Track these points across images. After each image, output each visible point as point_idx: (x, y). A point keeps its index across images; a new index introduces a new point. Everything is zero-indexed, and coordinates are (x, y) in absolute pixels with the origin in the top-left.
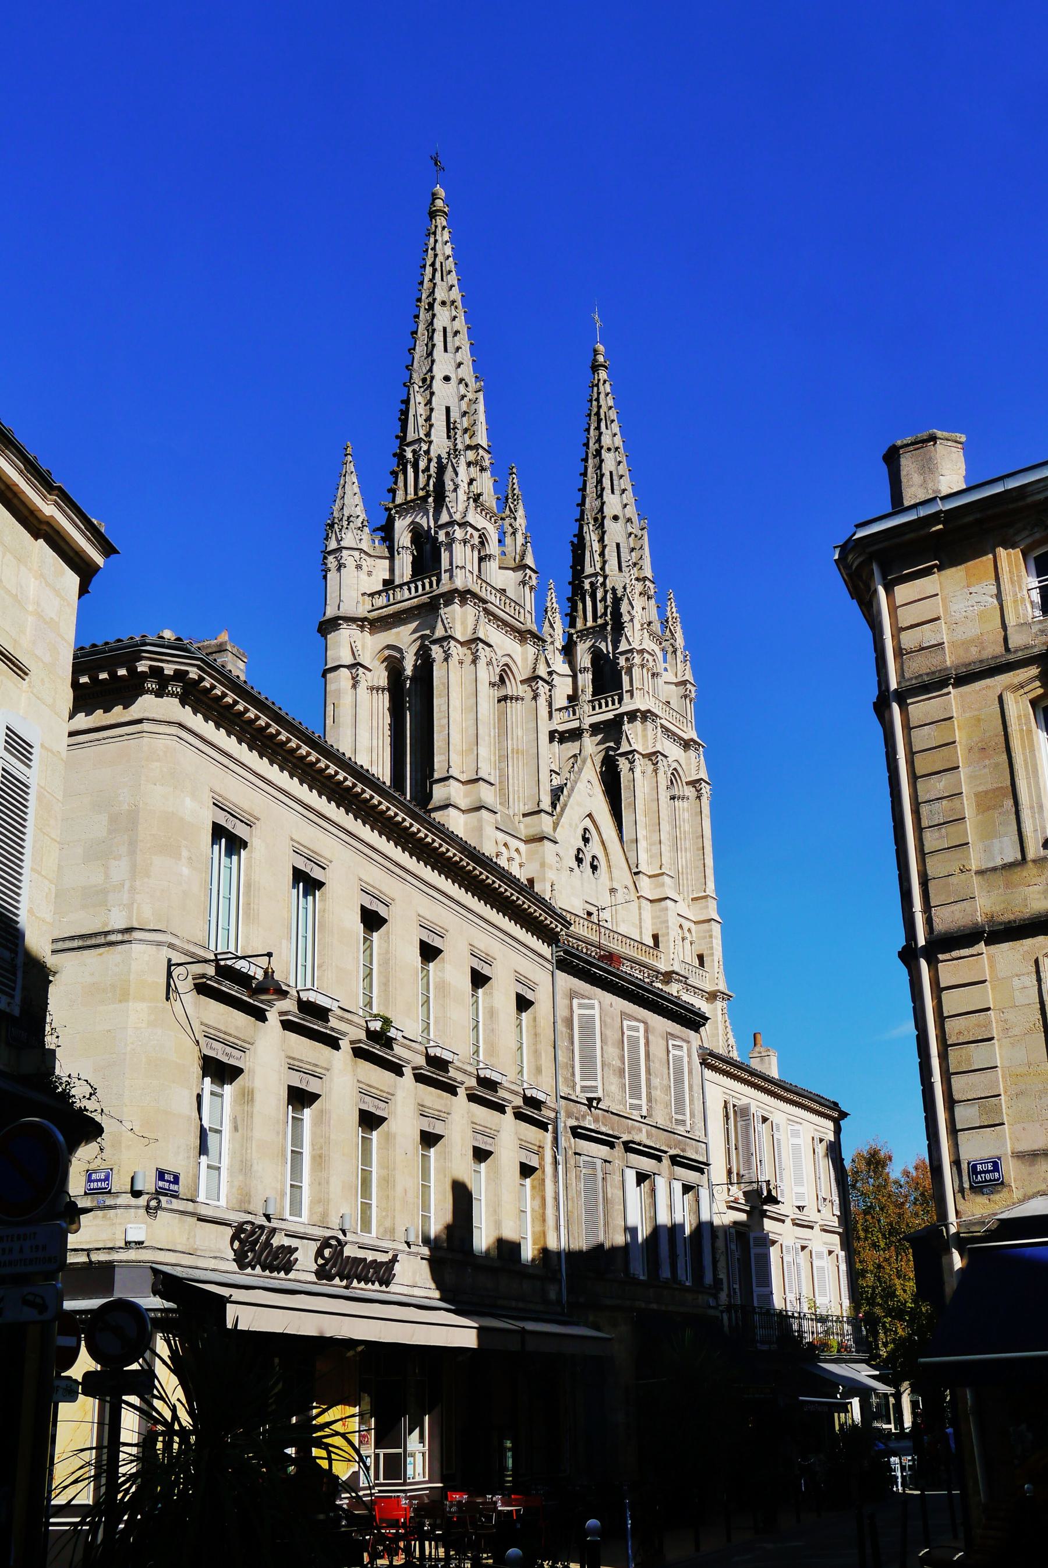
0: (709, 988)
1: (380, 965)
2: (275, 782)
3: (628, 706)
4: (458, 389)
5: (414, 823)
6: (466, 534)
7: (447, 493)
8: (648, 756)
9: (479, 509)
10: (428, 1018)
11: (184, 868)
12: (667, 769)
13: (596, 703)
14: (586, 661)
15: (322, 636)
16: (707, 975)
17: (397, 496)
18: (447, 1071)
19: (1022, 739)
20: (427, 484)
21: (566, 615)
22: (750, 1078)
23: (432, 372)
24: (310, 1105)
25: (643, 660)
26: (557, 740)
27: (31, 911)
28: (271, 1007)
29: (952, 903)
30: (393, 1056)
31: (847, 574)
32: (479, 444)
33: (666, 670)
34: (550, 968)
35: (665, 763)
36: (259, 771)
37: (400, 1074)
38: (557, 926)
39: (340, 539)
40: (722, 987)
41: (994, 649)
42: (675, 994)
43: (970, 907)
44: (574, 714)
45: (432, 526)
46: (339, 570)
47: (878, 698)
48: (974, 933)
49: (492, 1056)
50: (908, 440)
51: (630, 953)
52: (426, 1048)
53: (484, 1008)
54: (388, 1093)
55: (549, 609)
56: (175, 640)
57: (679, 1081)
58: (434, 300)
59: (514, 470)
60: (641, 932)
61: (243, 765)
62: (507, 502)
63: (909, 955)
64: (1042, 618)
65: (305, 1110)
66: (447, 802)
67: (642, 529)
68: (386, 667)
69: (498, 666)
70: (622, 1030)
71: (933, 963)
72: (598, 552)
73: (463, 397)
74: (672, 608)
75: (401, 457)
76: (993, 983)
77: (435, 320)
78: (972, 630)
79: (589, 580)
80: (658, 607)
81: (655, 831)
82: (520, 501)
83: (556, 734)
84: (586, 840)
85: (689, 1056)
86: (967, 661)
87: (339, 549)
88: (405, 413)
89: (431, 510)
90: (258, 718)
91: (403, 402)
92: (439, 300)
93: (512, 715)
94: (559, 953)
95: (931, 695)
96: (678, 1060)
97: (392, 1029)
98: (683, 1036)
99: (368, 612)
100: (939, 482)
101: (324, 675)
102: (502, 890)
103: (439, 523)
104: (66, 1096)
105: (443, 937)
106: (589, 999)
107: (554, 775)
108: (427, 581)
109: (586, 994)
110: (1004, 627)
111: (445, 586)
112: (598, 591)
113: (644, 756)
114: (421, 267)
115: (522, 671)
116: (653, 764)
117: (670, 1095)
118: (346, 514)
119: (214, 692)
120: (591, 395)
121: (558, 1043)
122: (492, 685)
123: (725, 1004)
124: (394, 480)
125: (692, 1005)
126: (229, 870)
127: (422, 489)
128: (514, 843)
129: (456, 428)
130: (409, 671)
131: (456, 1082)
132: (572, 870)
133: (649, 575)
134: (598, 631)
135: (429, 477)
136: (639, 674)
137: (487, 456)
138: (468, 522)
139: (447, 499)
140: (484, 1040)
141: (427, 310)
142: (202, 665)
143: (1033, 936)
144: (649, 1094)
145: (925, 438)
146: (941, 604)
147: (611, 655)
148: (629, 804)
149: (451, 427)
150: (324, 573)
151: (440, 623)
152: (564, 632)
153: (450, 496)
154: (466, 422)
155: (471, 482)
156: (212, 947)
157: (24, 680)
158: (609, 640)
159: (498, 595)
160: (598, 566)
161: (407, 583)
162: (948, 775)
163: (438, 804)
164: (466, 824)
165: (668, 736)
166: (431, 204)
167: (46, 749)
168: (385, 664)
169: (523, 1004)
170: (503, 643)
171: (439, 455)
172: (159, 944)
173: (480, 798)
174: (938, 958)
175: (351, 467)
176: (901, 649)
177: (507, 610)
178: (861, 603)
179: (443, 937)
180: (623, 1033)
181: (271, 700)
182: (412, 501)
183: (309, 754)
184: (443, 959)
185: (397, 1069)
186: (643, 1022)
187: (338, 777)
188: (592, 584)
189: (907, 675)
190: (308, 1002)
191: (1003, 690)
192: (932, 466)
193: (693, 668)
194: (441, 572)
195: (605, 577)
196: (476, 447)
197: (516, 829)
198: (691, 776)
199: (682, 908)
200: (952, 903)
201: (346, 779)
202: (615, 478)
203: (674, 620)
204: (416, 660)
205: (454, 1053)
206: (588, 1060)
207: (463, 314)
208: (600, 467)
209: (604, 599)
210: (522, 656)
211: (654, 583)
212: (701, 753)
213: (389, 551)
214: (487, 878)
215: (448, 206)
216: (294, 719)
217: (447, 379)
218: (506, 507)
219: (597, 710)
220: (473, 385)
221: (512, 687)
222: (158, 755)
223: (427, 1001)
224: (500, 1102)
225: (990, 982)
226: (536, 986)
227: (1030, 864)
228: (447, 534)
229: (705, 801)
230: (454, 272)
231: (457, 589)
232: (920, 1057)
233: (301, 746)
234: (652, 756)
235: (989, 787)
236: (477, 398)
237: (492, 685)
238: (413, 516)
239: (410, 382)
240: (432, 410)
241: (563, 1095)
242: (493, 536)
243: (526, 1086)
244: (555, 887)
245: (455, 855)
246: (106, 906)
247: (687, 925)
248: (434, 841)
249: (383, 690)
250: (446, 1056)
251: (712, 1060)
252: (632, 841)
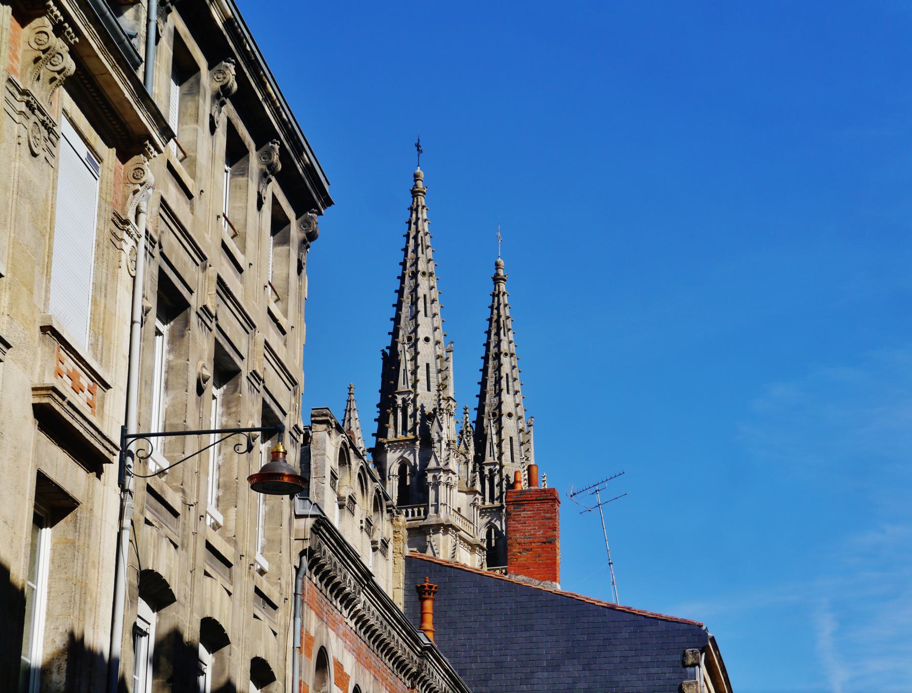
14: (483, 533)
79: (489, 467)
112: (496, 477)
147: (504, 533)
188: (404, 400)
194: (428, 505)
202: (510, 380)
207: (436, 281)
213: (380, 475)
215: (426, 187)
217: (427, 340)
228: (434, 477)
238: (402, 452)
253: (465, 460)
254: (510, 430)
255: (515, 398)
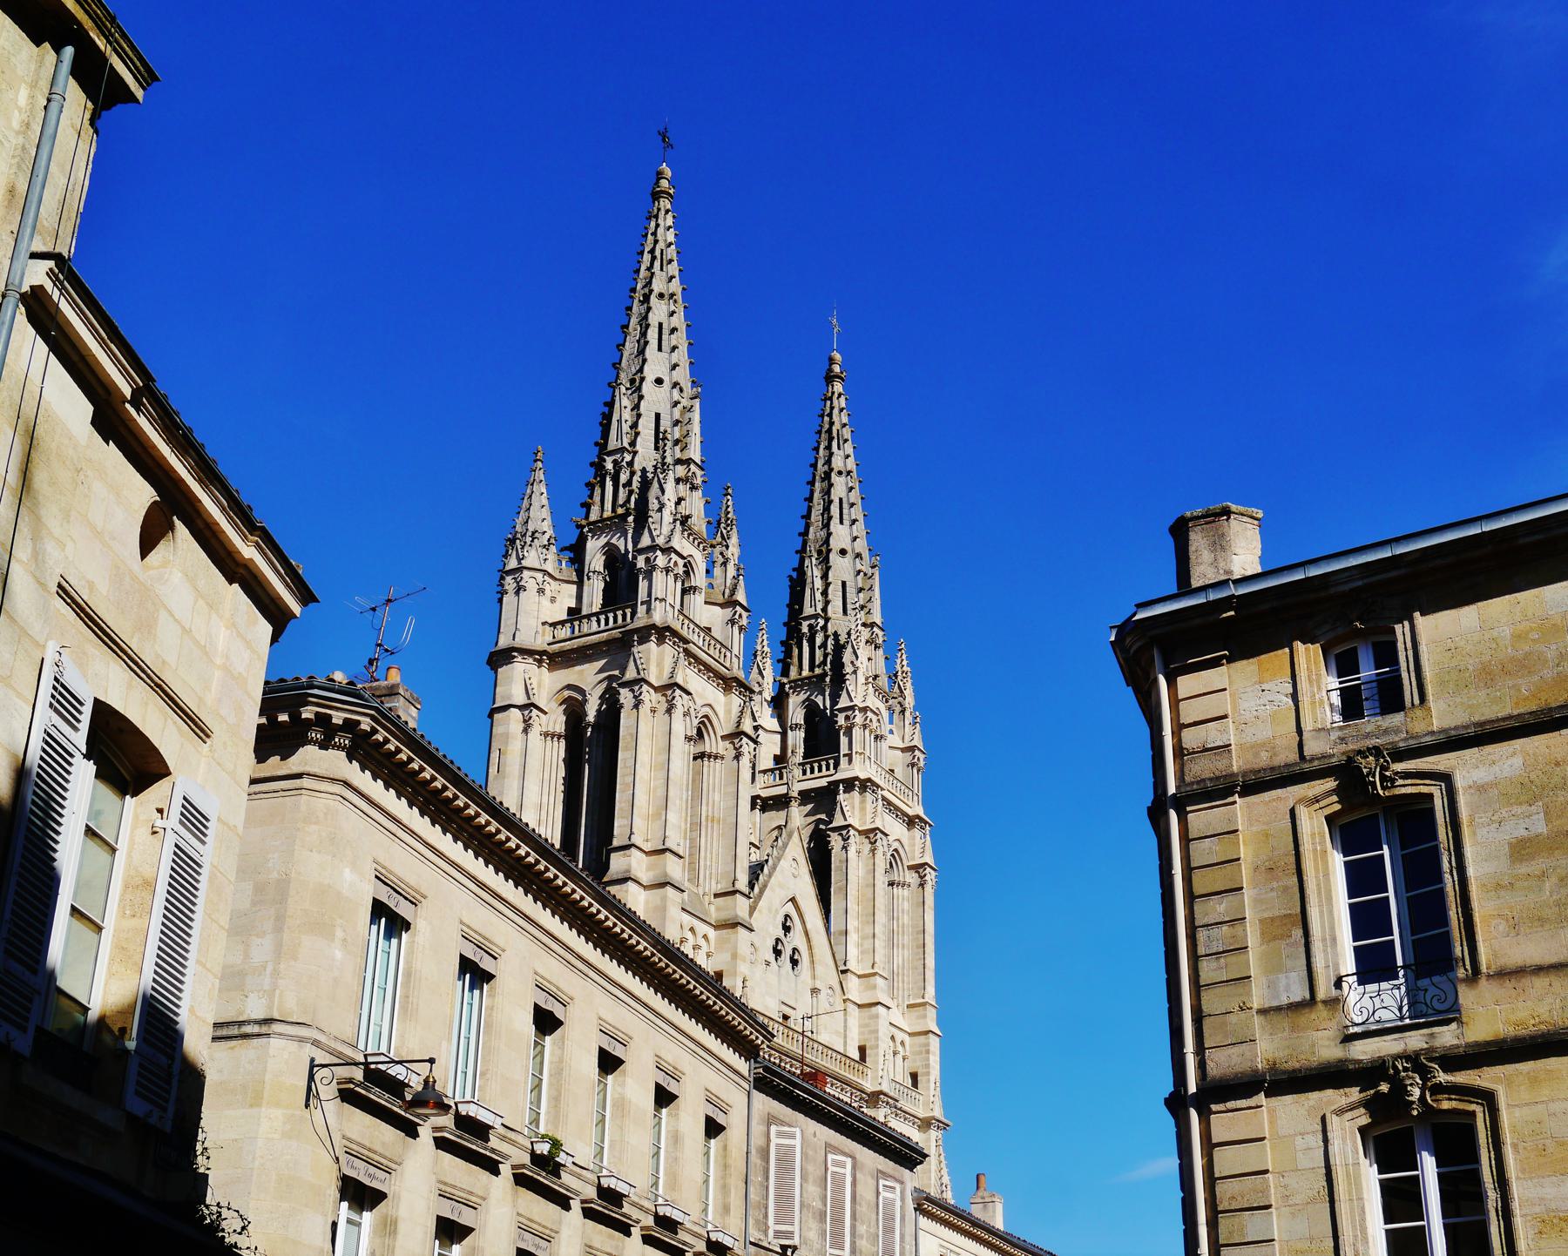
0: (922, 1113)
1: (551, 1075)
2: (447, 854)
3: (844, 773)
4: (671, 393)
5: (602, 909)
6: (669, 562)
7: (651, 513)
8: (865, 833)
9: (686, 533)
10: (603, 1142)
11: (337, 952)
12: (886, 849)
13: (808, 767)
15: (492, 669)
16: (921, 1098)
17: (592, 511)
18: (621, 1207)
19: (1315, 860)
20: (628, 501)
21: (779, 661)
22: (972, 1229)
23: (642, 373)
24: (460, 1241)
25: (866, 719)
26: (758, 807)
27: (192, 1010)
28: (425, 1121)
29: (1229, 1045)
30: (560, 1186)
31: (1123, 659)
32: (691, 459)
33: (891, 732)
34: (747, 1087)
35: (885, 843)
36: (430, 841)
37: (567, 1207)
38: (757, 1038)
39: (521, 557)
40: (938, 1113)
41: (1289, 756)
42: (882, 1120)
43: (1250, 1051)
44: (781, 778)
45: (630, 550)
46: (517, 593)
47: (1153, 802)
48: (1253, 1082)
49: (674, 1189)
50: (1198, 512)
51: (831, 1067)
52: (599, 1177)
53: (668, 1132)
54: (551, 1230)
55: (759, 653)
56: (347, 684)
57: (889, 1230)
58: (651, 291)
59: (730, 491)
60: (845, 1042)
61: (412, 833)
62: (719, 527)
63: (1177, 1103)
64: (1342, 724)
65: (454, 1246)
66: (626, 875)
67: (872, 567)
68: (564, 710)
69: (696, 717)
70: (826, 1165)
71: (1205, 1116)
72: (820, 591)
73: (676, 404)
74: (902, 660)
75: (599, 466)
76: (1273, 1141)
77: (650, 314)
78: (1263, 733)
79: (808, 622)
80: (886, 658)
81: (868, 922)
82: (734, 527)
83: (758, 801)
84: (787, 929)
85: (903, 1199)
86: (1256, 767)
87: (520, 569)
88: (608, 417)
89: (631, 531)
90: (434, 779)
91: (606, 404)
92: (656, 291)
93: (709, 775)
94: (758, 1070)
95: (1214, 804)
96: (889, 1204)
97: (562, 1154)
98: (897, 1175)
99: (549, 644)
100: (1231, 562)
101: (491, 716)
102: (697, 992)
103: (639, 547)
104: (215, 1228)
105: (625, 1046)
106: (790, 1126)
107: (753, 849)
108: (619, 613)
109: (787, 1120)
110: (1299, 731)
111: (641, 620)
113: (860, 833)
114: (638, 254)
115: (724, 725)
116: (871, 843)
117: (878, 1245)
118: (531, 529)
119: (387, 747)
120: (823, 410)
121: (751, 1177)
122: (689, 739)
123: (940, 1134)
124: (589, 493)
125: (909, 1138)
126: (387, 955)
127: (622, 506)
128: (702, 928)
129: (666, 438)
130: (591, 718)
131: (631, 1220)
132: (768, 963)
133: (878, 621)
134: (815, 683)
135: (631, 492)
136: (861, 735)
137: (699, 473)
138: (672, 547)
139: (650, 519)
140: (665, 1169)
141: (642, 303)
142: (376, 715)
143: (1321, 1088)
144: (853, 1243)
145: (1218, 511)
146: (1229, 701)
147: (828, 711)
148: (840, 889)
149: (659, 438)
150: (499, 596)
151: (631, 663)
152: (775, 680)
153: (654, 516)
154: (677, 434)
155: (679, 501)
156: (361, 1046)
157: (205, 743)
158: (827, 693)
159: (702, 634)
160: (820, 606)
161: (597, 614)
162: (1230, 897)
163: (615, 877)
164: (647, 902)
165: (890, 810)
166: (655, 184)
167: (224, 824)
168: (564, 707)
169: (713, 1129)
170: (704, 690)
171: (644, 468)
172: (302, 1040)
173: (666, 872)
174: (1210, 1108)
175: (540, 475)
176: (1182, 748)
177: (711, 652)
178: (1137, 692)
179: (625, 1046)
180: (826, 1169)
181: (449, 757)
182: (609, 519)
183: (488, 823)
184: (624, 1071)
185: (563, 1202)
186: (851, 1157)
187: (509, 844)
188: (811, 627)
189: (1187, 779)
190: (468, 1117)
191: (1296, 803)
192: (1224, 543)
193: (922, 731)
195: (827, 620)
196: (687, 462)
197: (707, 912)
198: (913, 859)
199: (896, 1016)
200: (1229, 1045)
201: (528, 854)
202: (845, 506)
203: (904, 675)
204: (601, 705)
205: (631, 1185)
206: (784, 1199)
207: (683, 309)
208: (828, 493)
209: (824, 645)
210: (725, 706)
211: (883, 631)
212: (928, 832)
214: (681, 977)
216: (473, 781)
217: (659, 381)
218: (717, 532)
219: (809, 775)
220: (689, 390)
221: (712, 744)
222: (317, 817)
223: (602, 1121)
224: (680, 1246)
225: (1269, 1140)
226: (729, 1108)
227: (1320, 1004)
228: (647, 560)
229: (929, 889)
230: (676, 262)
231: (654, 624)
232: (1185, 1224)
233: (459, 797)
234: (870, 834)
235: (1277, 913)
236: (692, 406)
237: (689, 739)
239: (616, 382)
240: (639, 416)
241: (752, 1240)
242: (700, 565)
243: (710, 1227)
244: (747, 984)
245: (646, 949)
246: (243, 990)
247: (900, 1036)
248: (623, 931)
249: (559, 737)
250: (622, 1188)
251: (929, 1206)
252: (840, 933)
253: (722, 560)
254: (842, 572)
255: (851, 529)
